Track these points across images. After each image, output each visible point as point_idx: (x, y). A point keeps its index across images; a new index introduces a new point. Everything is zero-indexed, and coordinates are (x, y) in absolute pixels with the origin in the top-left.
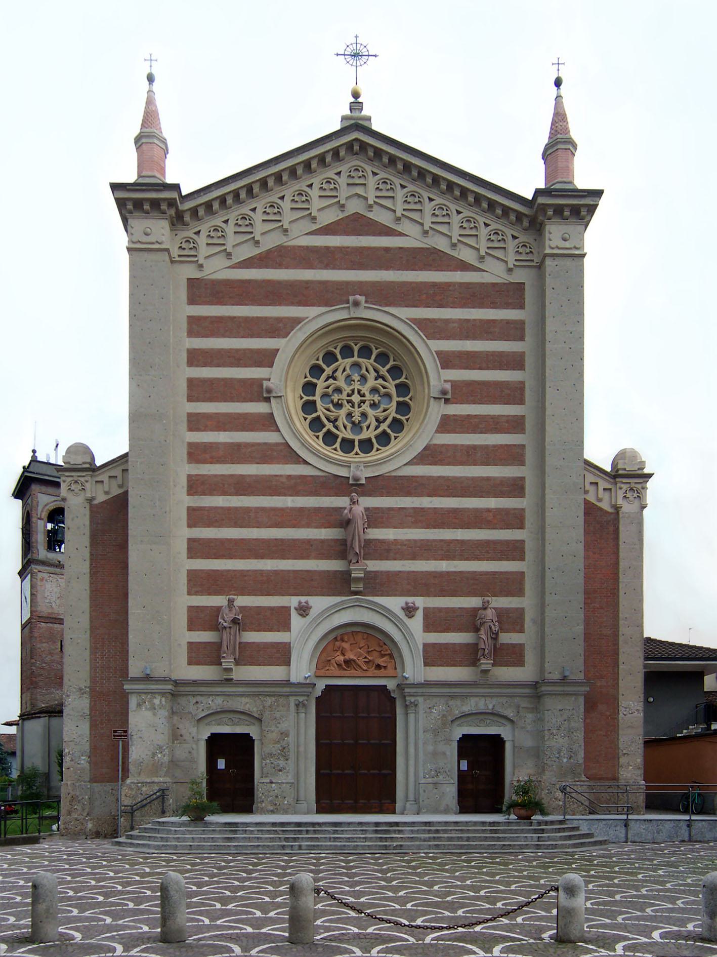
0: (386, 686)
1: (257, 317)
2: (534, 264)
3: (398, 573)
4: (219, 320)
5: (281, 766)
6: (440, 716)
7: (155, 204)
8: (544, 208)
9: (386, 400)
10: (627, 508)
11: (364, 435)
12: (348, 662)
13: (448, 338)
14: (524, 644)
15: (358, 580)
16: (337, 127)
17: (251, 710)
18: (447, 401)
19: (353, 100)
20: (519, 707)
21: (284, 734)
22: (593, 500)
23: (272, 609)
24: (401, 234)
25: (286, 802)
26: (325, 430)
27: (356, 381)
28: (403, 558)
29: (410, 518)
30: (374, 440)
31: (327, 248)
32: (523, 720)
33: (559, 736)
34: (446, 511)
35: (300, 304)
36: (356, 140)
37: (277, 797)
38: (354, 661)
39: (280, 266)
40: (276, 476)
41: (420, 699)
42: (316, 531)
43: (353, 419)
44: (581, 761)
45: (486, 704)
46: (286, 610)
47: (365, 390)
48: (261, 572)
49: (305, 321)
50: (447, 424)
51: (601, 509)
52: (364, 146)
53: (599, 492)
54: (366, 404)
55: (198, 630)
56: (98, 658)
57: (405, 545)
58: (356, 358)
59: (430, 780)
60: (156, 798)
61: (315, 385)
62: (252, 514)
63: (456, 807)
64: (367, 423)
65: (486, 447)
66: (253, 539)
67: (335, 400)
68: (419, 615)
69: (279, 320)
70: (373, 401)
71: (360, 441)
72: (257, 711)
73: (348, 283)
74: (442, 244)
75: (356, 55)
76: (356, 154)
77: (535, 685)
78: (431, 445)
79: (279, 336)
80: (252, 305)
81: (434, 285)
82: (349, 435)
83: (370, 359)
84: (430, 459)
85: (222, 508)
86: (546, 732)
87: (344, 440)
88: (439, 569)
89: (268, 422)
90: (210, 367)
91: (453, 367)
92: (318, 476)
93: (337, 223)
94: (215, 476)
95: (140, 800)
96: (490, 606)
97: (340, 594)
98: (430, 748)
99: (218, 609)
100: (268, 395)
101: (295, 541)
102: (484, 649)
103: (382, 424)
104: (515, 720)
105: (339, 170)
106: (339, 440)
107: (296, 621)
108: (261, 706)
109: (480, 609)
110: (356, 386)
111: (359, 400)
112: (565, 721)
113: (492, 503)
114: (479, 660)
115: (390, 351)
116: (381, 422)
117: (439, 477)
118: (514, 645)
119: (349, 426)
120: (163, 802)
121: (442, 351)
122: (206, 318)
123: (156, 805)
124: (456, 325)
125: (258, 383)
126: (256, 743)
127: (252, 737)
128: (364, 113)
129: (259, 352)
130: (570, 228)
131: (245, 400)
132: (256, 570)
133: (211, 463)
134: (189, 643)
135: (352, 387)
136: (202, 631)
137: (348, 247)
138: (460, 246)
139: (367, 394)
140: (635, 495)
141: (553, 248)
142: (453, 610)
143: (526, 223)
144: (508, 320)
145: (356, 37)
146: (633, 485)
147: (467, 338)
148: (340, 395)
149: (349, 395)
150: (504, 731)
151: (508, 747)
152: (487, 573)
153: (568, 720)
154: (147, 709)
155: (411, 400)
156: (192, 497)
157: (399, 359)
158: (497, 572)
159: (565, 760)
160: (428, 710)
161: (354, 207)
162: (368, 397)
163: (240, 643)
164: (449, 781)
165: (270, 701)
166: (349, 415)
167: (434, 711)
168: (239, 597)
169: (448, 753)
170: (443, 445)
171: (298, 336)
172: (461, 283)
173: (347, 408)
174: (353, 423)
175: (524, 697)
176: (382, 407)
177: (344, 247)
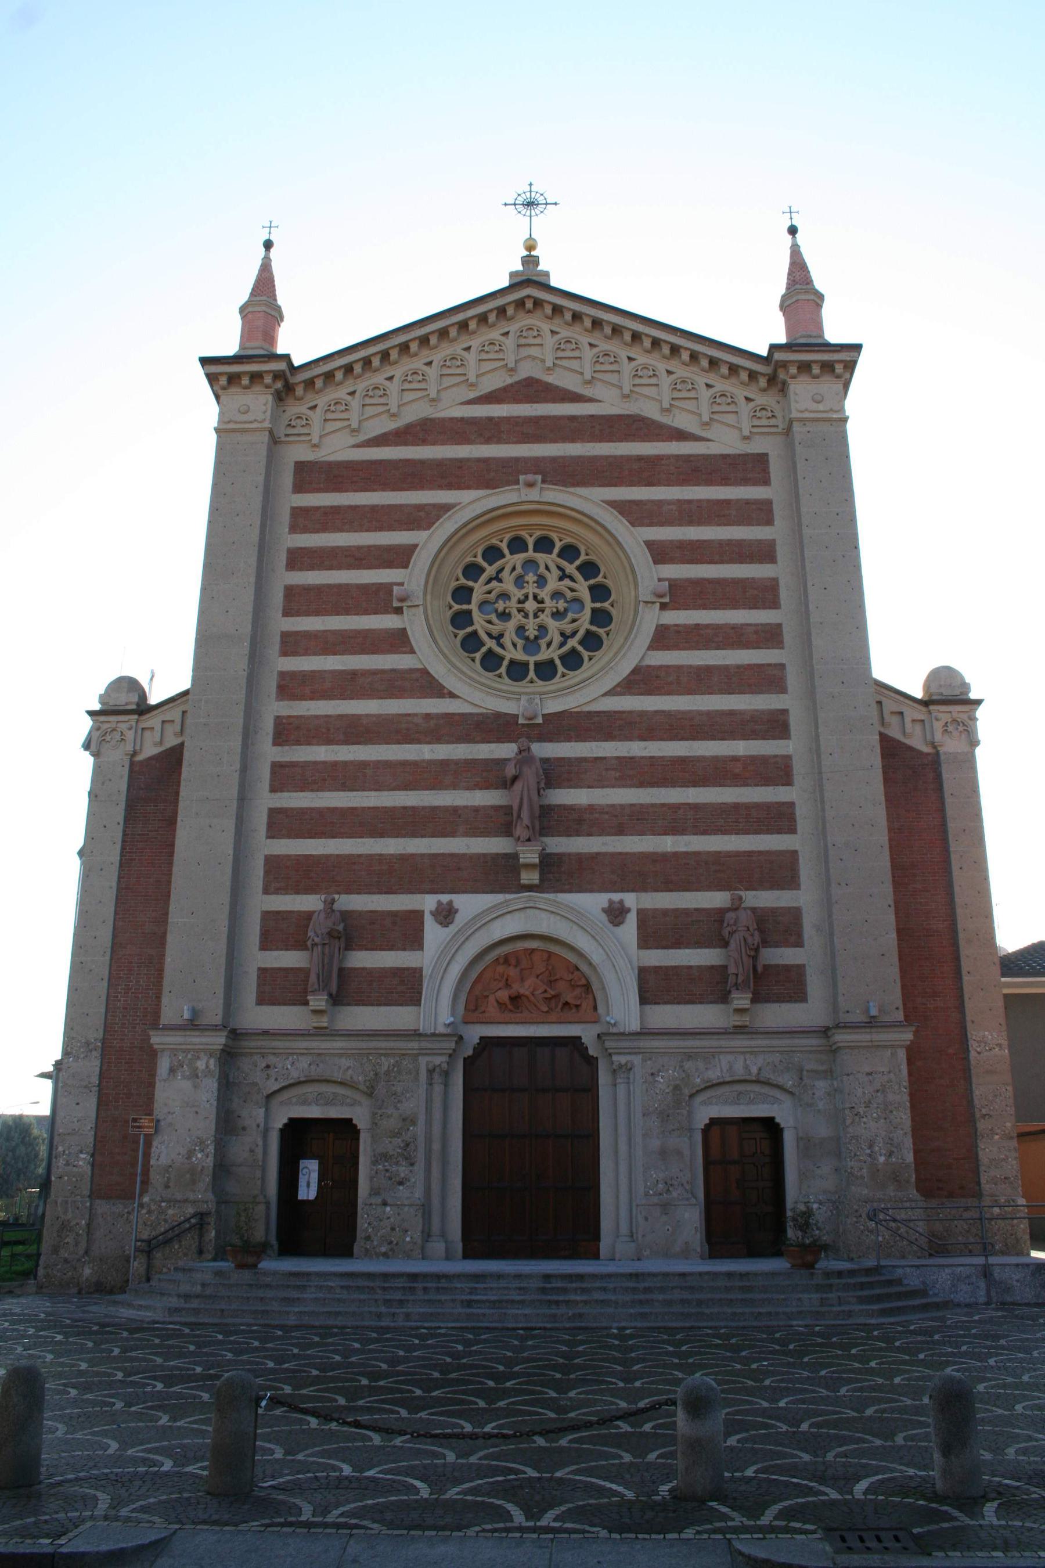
0: (580, 1038)
1: (389, 506)
2: (779, 430)
3: (595, 857)
4: (336, 510)
5: (402, 1175)
6: (671, 1088)
7: (256, 377)
8: (784, 365)
9: (576, 606)
10: (950, 746)
11: (543, 655)
12: (515, 999)
13: (662, 524)
14: (804, 966)
15: (529, 866)
16: (505, 283)
17: (355, 1078)
18: (663, 607)
19: (526, 253)
20: (802, 1070)
21: (409, 1121)
22: (899, 736)
23: (394, 914)
24: (590, 400)
25: (408, 1239)
26: (484, 649)
27: (531, 582)
28: (602, 832)
29: (613, 772)
30: (558, 662)
31: (490, 419)
32: (810, 1092)
33: (869, 1117)
34: (668, 761)
35: (450, 487)
36: (529, 297)
37: (393, 1229)
38: (527, 997)
39: (424, 442)
40: (409, 715)
41: (637, 1060)
42: (467, 794)
43: (527, 634)
44: (910, 1158)
45: (746, 1067)
46: (415, 918)
47: (544, 594)
48: (381, 858)
49: (455, 509)
50: (663, 638)
51: (910, 749)
52: (538, 303)
53: (906, 726)
54: (545, 613)
55: (277, 949)
56: (120, 993)
57: (607, 813)
58: (531, 553)
59: (655, 1200)
60: (190, 1229)
61: (471, 590)
62: (369, 772)
63: (702, 1246)
64: (548, 639)
65: (726, 668)
66: (369, 808)
67: (500, 609)
68: (632, 919)
69: (419, 507)
70: (557, 608)
71: (537, 664)
72: (365, 1081)
73: (517, 460)
74: (651, 411)
75: (530, 204)
76: (529, 311)
77: (825, 1032)
78: (642, 666)
79: (419, 528)
80: (383, 490)
81: (639, 458)
82: (520, 656)
83: (550, 553)
84: (642, 686)
85: (324, 763)
86: (847, 1112)
87: (512, 662)
88: (660, 849)
89: (399, 641)
90: (319, 570)
91: (672, 561)
92: (471, 714)
93: (505, 389)
94: (317, 717)
95: (162, 1230)
96: (743, 905)
97: (502, 890)
98: (655, 1143)
99: (309, 915)
100: (399, 605)
101: (434, 809)
102: (737, 975)
103: (570, 640)
104: (796, 1091)
105: (506, 330)
106: (505, 663)
107: (433, 933)
108: (372, 1073)
109: (728, 910)
110: (531, 588)
111: (535, 608)
112: (878, 1091)
113: (740, 748)
114: (730, 992)
115: (580, 541)
116: (568, 637)
117: (656, 712)
118: (788, 968)
119: (520, 643)
120: (201, 1236)
121: (654, 541)
122: (317, 508)
123: (190, 1241)
124: (674, 507)
125: (386, 589)
126: (363, 1136)
127: (356, 1126)
128: (540, 268)
129: (389, 549)
130: (827, 386)
131: (366, 612)
132: (371, 855)
133: (312, 699)
134: (259, 969)
135: (524, 591)
136: (281, 950)
137: (519, 417)
138: (676, 411)
139: (547, 600)
140: (961, 728)
141: (802, 412)
142: (686, 912)
143: (763, 382)
144: (747, 500)
145: (531, 185)
146: (955, 715)
147: (691, 523)
148: (507, 602)
149: (520, 602)
150: (783, 1112)
151: (789, 1139)
152: (738, 854)
153: (882, 1090)
154: (184, 1077)
155: (612, 606)
156: (280, 748)
157: (594, 552)
158: (752, 852)
159: (882, 1159)
160: (650, 1079)
161: (526, 371)
162: (549, 603)
163: (341, 970)
164: (687, 1199)
165: (387, 1064)
166: (521, 630)
167: (660, 1079)
168: (342, 896)
169: (687, 1152)
170: (660, 667)
171: (446, 527)
172: (678, 456)
173: (517, 619)
174: (527, 639)
175: (811, 1052)
176: (570, 616)
177: (513, 417)
